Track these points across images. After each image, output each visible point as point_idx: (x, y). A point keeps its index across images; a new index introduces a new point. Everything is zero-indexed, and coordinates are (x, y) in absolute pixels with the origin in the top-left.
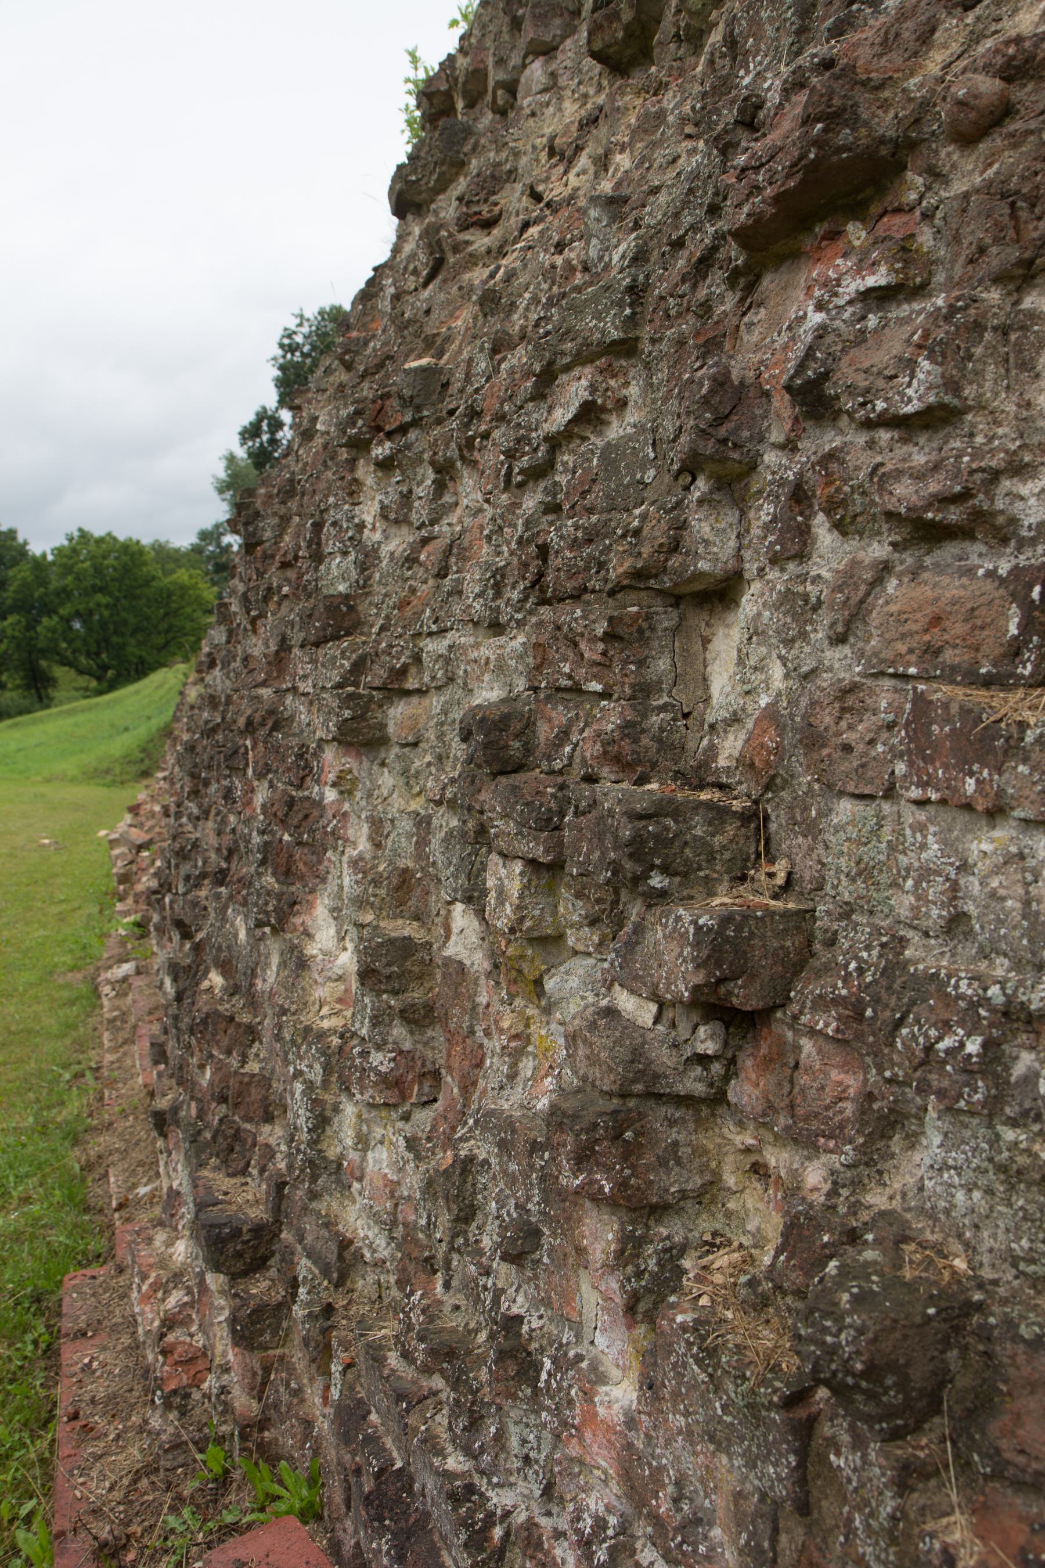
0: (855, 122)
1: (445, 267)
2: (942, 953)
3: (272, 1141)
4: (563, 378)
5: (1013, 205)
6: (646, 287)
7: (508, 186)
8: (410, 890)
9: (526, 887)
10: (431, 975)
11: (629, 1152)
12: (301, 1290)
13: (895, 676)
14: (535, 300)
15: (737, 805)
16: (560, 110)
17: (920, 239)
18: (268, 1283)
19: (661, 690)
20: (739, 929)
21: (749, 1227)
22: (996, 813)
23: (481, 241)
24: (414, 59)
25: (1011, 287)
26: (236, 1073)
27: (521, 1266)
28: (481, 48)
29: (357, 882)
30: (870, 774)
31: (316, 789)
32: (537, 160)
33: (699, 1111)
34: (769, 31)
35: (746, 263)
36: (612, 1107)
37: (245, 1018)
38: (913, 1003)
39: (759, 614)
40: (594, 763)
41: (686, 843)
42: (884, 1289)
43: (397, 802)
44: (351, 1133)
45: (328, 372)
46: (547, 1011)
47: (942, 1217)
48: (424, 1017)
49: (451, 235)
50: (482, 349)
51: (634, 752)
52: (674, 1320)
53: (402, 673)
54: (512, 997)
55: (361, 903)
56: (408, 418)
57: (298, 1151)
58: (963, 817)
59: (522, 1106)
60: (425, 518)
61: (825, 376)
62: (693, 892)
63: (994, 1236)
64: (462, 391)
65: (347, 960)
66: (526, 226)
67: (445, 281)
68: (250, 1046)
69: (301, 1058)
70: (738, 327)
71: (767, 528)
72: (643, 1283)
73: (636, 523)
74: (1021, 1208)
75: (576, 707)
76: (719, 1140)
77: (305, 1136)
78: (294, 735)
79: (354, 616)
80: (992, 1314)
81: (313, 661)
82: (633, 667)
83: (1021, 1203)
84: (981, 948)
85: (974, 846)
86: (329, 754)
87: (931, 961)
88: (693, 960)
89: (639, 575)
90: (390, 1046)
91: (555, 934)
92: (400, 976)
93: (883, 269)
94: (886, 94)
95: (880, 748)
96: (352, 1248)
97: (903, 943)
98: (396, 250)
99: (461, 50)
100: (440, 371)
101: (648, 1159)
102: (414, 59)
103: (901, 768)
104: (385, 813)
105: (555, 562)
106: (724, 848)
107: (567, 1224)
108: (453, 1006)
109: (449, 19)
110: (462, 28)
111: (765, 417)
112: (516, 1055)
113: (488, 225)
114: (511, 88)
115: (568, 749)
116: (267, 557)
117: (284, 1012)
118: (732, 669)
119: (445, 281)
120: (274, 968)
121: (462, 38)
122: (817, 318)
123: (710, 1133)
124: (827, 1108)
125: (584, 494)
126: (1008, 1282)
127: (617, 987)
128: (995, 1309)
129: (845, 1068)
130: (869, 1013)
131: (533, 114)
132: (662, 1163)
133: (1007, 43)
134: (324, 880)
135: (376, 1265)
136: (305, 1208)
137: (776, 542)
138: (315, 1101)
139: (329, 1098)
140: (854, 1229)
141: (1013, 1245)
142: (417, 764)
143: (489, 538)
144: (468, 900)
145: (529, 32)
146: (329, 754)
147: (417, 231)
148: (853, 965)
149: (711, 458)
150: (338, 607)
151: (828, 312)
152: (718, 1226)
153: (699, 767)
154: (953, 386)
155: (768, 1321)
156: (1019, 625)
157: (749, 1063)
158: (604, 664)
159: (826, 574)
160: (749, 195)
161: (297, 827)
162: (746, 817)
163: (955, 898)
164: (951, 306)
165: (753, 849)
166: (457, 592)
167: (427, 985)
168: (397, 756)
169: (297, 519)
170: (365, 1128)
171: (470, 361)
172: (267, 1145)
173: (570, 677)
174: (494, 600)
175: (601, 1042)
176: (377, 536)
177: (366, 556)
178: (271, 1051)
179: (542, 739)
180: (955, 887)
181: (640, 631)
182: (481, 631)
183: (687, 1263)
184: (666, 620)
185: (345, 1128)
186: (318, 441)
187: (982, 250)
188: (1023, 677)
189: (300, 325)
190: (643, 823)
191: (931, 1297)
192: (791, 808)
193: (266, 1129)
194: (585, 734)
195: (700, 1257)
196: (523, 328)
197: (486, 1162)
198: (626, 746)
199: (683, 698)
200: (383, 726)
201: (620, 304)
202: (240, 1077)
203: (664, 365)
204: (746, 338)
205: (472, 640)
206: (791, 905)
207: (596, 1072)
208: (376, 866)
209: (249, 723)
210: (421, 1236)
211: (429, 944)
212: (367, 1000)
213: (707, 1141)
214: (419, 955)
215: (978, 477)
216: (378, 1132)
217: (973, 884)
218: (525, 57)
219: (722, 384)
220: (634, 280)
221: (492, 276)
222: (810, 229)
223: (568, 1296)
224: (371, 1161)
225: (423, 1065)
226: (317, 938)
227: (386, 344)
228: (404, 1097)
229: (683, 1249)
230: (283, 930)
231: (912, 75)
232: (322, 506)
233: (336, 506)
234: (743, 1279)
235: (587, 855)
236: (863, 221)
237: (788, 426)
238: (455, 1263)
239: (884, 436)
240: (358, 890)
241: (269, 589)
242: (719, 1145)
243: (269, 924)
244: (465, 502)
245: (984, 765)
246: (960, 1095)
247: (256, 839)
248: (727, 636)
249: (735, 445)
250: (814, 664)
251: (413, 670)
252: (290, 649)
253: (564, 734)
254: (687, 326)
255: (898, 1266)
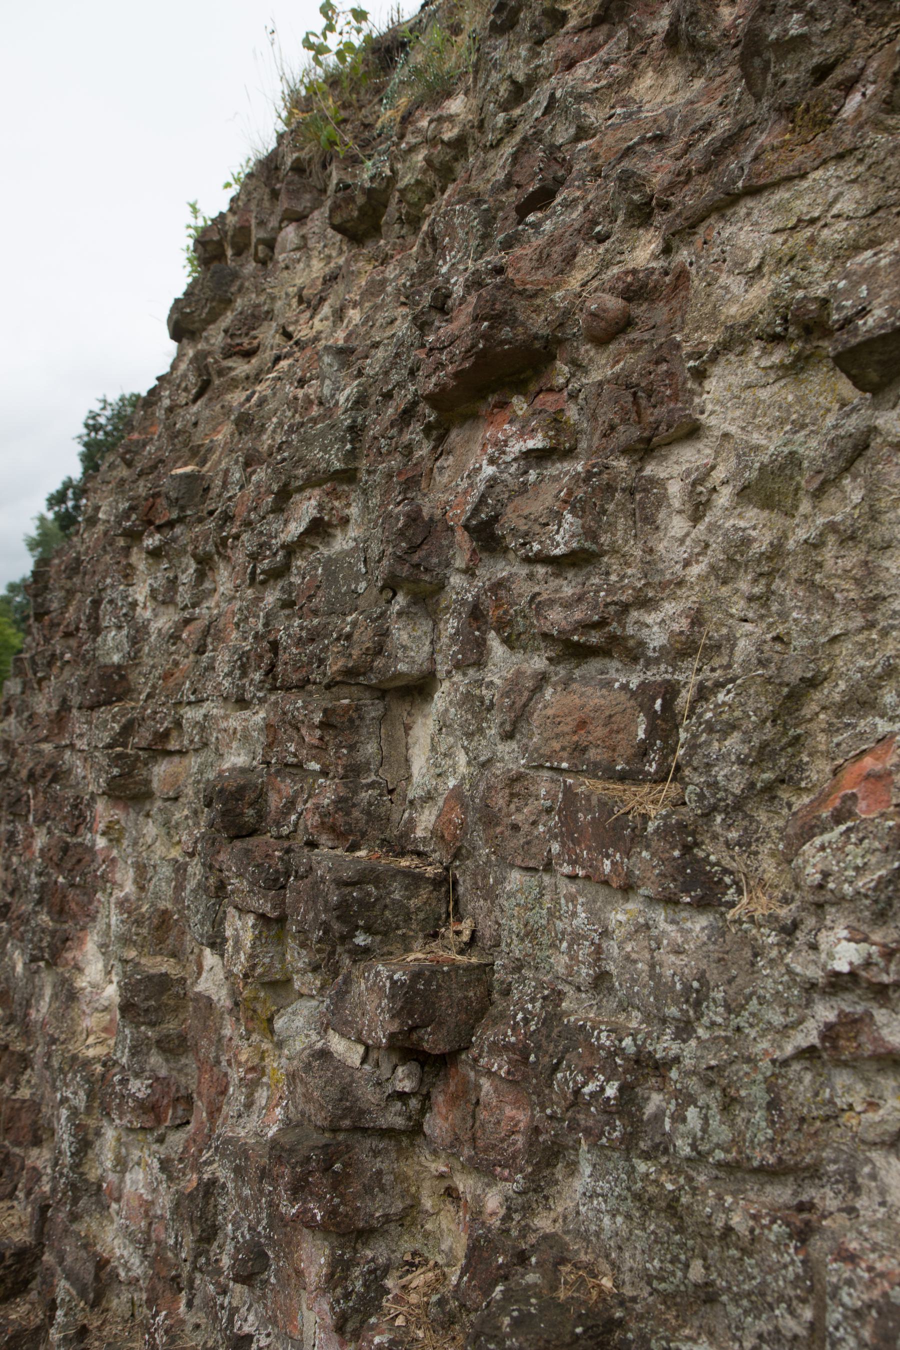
0: (514, 322)
1: (211, 387)
2: (591, 1006)
3: (40, 1164)
4: (297, 497)
5: (635, 394)
6: (364, 428)
7: (266, 323)
8: (169, 929)
9: (257, 938)
10: (185, 1007)
11: (338, 1182)
12: (59, 1313)
13: (551, 768)
14: (280, 424)
15: (430, 871)
16: (309, 266)
17: (568, 414)
18: (28, 1306)
19: (369, 770)
20: (428, 983)
21: (443, 1247)
22: (628, 889)
23: (241, 368)
24: (195, 210)
25: (635, 457)
26: (8, 1099)
27: (251, 1286)
28: (246, 209)
29: (122, 922)
30: (534, 850)
31: (89, 836)
32: (290, 305)
33: (401, 1141)
34: (461, 234)
35: (437, 420)
36: (324, 1141)
37: (19, 1047)
38: (566, 1050)
39: (447, 710)
40: (314, 831)
41: (386, 906)
42: (540, 1311)
43: (160, 850)
44: (110, 1155)
45: (112, 467)
46: (280, 1045)
47: (593, 1239)
48: (179, 1046)
49: (216, 362)
50: (237, 462)
51: (346, 823)
52: (372, 1341)
53: (166, 735)
54: (249, 1032)
55: (125, 941)
56: (174, 515)
57: (62, 1174)
58: (603, 891)
59: (256, 1134)
60: (187, 602)
61: (495, 519)
62: (392, 949)
63: (633, 1257)
64: (220, 495)
65: (111, 992)
66: (278, 359)
67: (210, 399)
68: (23, 1073)
69: (67, 1086)
70: (432, 470)
71: (452, 637)
72: (351, 1304)
73: (348, 629)
74: (653, 1232)
75: (302, 781)
76: (417, 1168)
77: (68, 1160)
78: (71, 786)
79: (124, 684)
80: (630, 1330)
81: (89, 723)
82: (345, 751)
83: (652, 1227)
84: (620, 1003)
85: (612, 916)
86: (100, 806)
87: (582, 1014)
88: (390, 1010)
89: (350, 674)
90: (147, 1074)
91: (284, 978)
92: (157, 1009)
93: (540, 436)
94: (539, 301)
95: (541, 829)
96: (108, 1268)
97: (561, 995)
98: (174, 367)
99: (231, 210)
100: (203, 478)
101: (355, 1187)
102: (195, 210)
103: (556, 847)
104: (149, 859)
105: (283, 657)
106: (419, 909)
107: (289, 1247)
108: (202, 1038)
109: (224, 181)
110: (235, 190)
111: (450, 546)
112: (252, 1086)
113: (248, 354)
114: (270, 244)
115: (293, 817)
116: (53, 625)
117: (54, 1041)
118: (428, 754)
119: (210, 399)
120: (47, 999)
121: (233, 200)
122: (489, 470)
123: (410, 1161)
124: (502, 1141)
125: (310, 598)
126: (645, 1299)
127: (331, 1032)
128: (632, 1325)
129: (516, 1104)
130: (532, 1058)
131: (287, 268)
132: (368, 1190)
133: (626, 273)
134: (94, 919)
135: (130, 1283)
136: (66, 1230)
137: (459, 652)
138: (78, 1126)
139: (92, 1123)
140: (523, 1251)
141: (648, 1265)
142: (177, 816)
143: (237, 625)
144: (212, 945)
145: (284, 203)
146: (100, 806)
147: (191, 353)
148: (520, 1016)
149: (407, 579)
150: (111, 676)
151: (498, 466)
152: (418, 1246)
153: (401, 837)
154: (591, 534)
155: (454, 1338)
156: (646, 730)
157: (441, 1099)
158: (321, 747)
159: (497, 681)
160: (436, 369)
161: (70, 871)
162: (437, 882)
163: (599, 959)
164: (588, 471)
165: (443, 910)
166: (211, 668)
167: (181, 1017)
168: (160, 810)
169: (79, 595)
170: (123, 1150)
171: (227, 472)
172: (34, 1169)
173: (295, 756)
174: (240, 679)
175: (314, 1081)
176: (148, 614)
177: (137, 631)
178: (41, 1077)
179: (273, 808)
180: (599, 950)
181: (351, 721)
182: (230, 705)
183: (389, 1283)
184: (373, 710)
185: (105, 1151)
186: (100, 528)
187: (612, 428)
188: (649, 773)
189: (104, 408)
190: (349, 889)
191: (580, 1316)
192: (475, 875)
193: (35, 1152)
194: (308, 805)
195: (401, 1277)
196: (271, 447)
197: (224, 1186)
198: (340, 818)
199: (388, 777)
200: (148, 782)
201: (343, 440)
202: (11, 1104)
203: (377, 492)
204: (438, 479)
205: (222, 712)
206: (474, 960)
207: (311, 1109)
208: (140, 907)
209: (31, 775)
210: (170, 1254)
211: (184, 979)
212: (127, 1031)
213: (407, 1168)
214: (174, 990)
215: (612, 608)
216: (136, 1154)
217: (612, 947)
218: (281, 221)
219: (414, 520)
220: (354, 421)
221: (248, 399)
222: (484, 398)
223: (291, 1315)
224: (128, 1182)
225: (178, 1090)
226: (87, 972)
227: (159, 449)
228: (159, 1121)
229: (386, 1270)
230: (56, 964)
231: (558, 288)
232: (101, 586)
233: (113, 586)
234: (434, 1298)
235: (304, 915)
236: (525, 395)
237: (467, 556)
238: (198, 1282)
239: (541, 570)
240: (123, 929)
241: (53, 655)
242: (418, 1172)
243: (43, 959)
244: (221, 589)
245: (616, 849)
246: (602, 1133)
247: (34, 881)
248: (424, 724)
249: (426, 569)
250: (490, 755)
251: (175, 734)
252: (69, 709)
253: (291, 804)
254: (395, 462)
255: (554, 1288)
